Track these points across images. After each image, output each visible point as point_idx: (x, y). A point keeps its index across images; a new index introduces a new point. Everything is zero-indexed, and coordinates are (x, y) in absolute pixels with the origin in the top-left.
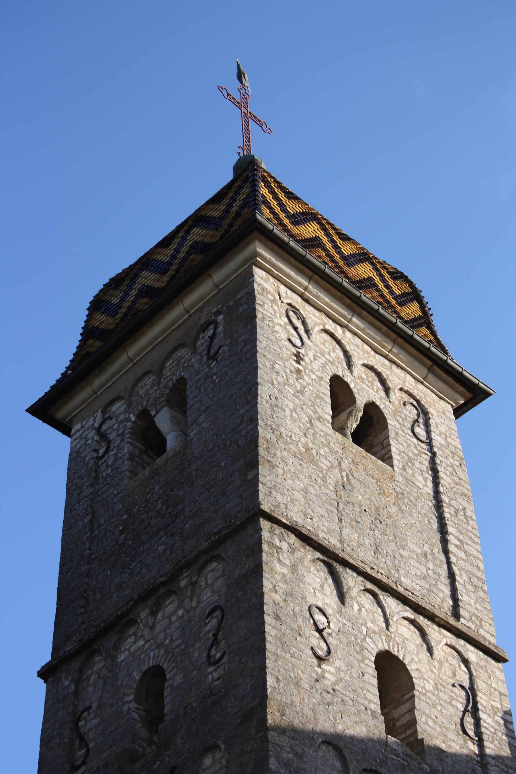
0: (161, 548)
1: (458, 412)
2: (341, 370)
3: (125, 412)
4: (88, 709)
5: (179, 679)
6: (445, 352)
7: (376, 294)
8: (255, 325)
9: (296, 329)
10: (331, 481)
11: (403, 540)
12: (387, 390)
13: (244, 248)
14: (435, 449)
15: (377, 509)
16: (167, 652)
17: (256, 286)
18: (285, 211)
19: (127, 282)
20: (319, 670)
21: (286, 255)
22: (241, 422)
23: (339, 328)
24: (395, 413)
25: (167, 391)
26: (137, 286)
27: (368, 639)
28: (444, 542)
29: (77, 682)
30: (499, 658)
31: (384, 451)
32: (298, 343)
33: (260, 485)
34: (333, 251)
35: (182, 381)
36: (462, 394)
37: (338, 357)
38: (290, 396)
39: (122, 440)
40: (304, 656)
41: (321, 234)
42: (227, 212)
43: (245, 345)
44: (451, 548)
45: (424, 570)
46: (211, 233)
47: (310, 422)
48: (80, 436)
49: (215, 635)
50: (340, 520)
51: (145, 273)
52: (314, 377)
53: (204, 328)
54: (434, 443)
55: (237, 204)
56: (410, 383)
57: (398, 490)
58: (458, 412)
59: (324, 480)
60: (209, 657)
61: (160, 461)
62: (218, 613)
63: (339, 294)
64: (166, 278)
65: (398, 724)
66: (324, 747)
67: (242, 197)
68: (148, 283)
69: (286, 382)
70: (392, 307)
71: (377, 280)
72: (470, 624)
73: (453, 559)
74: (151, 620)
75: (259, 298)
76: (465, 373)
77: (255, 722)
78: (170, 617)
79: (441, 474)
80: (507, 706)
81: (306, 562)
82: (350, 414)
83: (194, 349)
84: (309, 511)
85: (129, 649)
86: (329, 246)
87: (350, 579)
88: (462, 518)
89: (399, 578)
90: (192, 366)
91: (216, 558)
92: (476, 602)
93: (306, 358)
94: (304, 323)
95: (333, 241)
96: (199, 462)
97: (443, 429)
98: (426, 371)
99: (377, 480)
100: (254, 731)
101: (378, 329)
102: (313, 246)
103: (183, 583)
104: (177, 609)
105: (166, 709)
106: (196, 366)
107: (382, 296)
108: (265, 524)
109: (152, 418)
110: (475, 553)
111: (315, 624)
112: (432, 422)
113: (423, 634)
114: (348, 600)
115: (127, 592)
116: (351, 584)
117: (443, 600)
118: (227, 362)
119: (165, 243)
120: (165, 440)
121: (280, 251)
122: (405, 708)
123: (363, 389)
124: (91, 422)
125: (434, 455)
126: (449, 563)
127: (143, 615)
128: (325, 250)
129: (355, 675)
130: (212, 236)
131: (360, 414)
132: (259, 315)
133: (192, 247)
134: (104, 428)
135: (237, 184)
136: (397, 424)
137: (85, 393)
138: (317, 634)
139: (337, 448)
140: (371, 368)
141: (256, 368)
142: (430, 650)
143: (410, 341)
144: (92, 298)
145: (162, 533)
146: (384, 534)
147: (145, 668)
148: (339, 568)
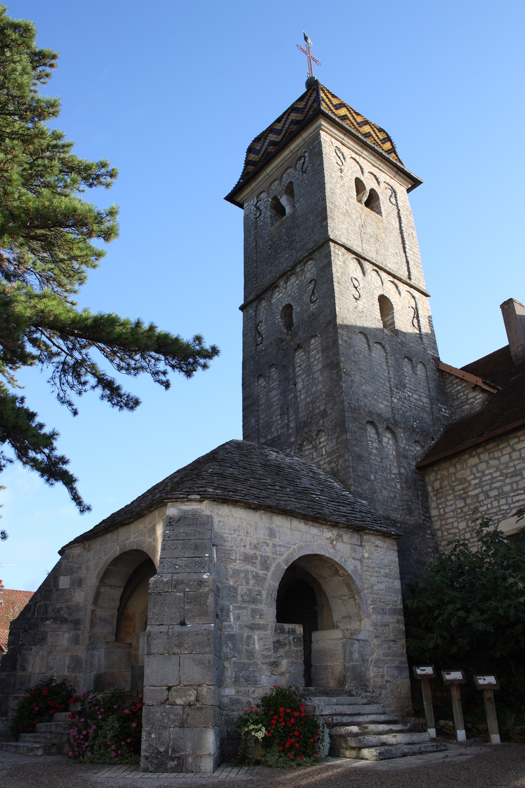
0: (287, 256)
1: (409, 191)
2: (359, 175)
3: (267, 197)
4: (261, 322)
5: (298, 309)
6: (402, 164)
7: (372, 139)
8: (322, 157)
9: (339, 158)
10: (357, 224)
11: (387, 248)
12: (379, 183)
13: (315, 122)
14: (399, 208)
15: (376, 235)
16: (293, 298)
17: (322, 140)
18: (332, 104)
19: (263, 139)
20: (356, 304)
21: (334, 125)
22: (319, 201)
23: (357, 156)
24: (383, 192)
25: (285, 188)
26: (267, 141)
27: (375, 290)
28: (404, 248)
29: (256, 311)
30: (427, 295)
31: (378, 210)
32: (341, 164)
33: (329, 228)
34: (353, 121)
35: (291, 183)
36: (410, 183)
37: (358, 169)
38: (339, 188)
39: (266, 210)
40: (350, 298)
41: (348, 113)
42: (306, 105)
43: (318, 167)
44: (407, 250)
45: (396, 260)
46: (300, 115)
47: (348, 199)
48: (248, 209)
49: (313, 291)
50: (362, 241)
51: (270, 135)
52: (348, 179)
53: (300, 159)
54: (399, 205)
55: (310, 102)
56: (388, 180)
57: (385, 226)
58: (409, 191)
59: (355, 224)
60: (311, 300)
61: (284, 218)
62: (313, 282)
63: (357, 141)
64: (280, 137)
65: (387, 323)
66: (359, 334)
67: (312, 98)
68: (273, 139)
69: (337, 182)
70: (379, 145)
71: (372, 133)
72: (415, 282)
73: (408, 255)
74: (285, 285)
75: (323, 145)
76: (412, 174)
77: (332, 325)
78: (293, 284)
79: (402, 219)
80: (430, 314)
81: (349, 259)
82: (364, 194)
83: (296, 169)
84: (349, 238)
85: (276, 298)
86: (351, 118)
87: (367, 266)
88: (411, 237)
89: (386, 264)
90: (295, 176)
91: (311, 259)
92: (418, 272)
93: (344, 171)
94: (343, 155)
95: (353, 116)
96: (301, 218)
97: (402, 199)
98: (395, 173)
99: (376, 223)
100: (332, 329)
101: (374, 156)
102: (345, 119)
103: (298, 270)
104: (296, 281)
105: (294, 321)
106: (297, 176)
107: (375, 140)
108: (332, 244)
109: (279, 200)
110: (417, 252)
111: (354, 285)
112: (397, 196)
113: (397, 287)
114: (366, 274)
115: (274, 274)
116: (368, 267)
117: (404, 272)
118: (311, 174)
119: (278, 120)
120: (285, 209)
121: (331, 123)
122: (390, 317)
123: (369, 183)
124: (252, 202)
125: (399, 210)
126: (406, 257)
127: (281, 284)
128: (350, 121)
129: (370, 305)
130: (300, 117)
131: (368, 194)
132: (324, 153)
133: (291, 122)
134: (258, 205)
135: (310, 92)
136: (383, 198)
137: (248, 190)
138: (355, 289)
139: (359, 209)
140: (372, 173)
141: (324, 176)
142: (400, 293)
143: (388, 160)
144: (247, 147)
145: (287, 249)
146: (380, 246)
147: (284, 305)
148: (362, 261)
